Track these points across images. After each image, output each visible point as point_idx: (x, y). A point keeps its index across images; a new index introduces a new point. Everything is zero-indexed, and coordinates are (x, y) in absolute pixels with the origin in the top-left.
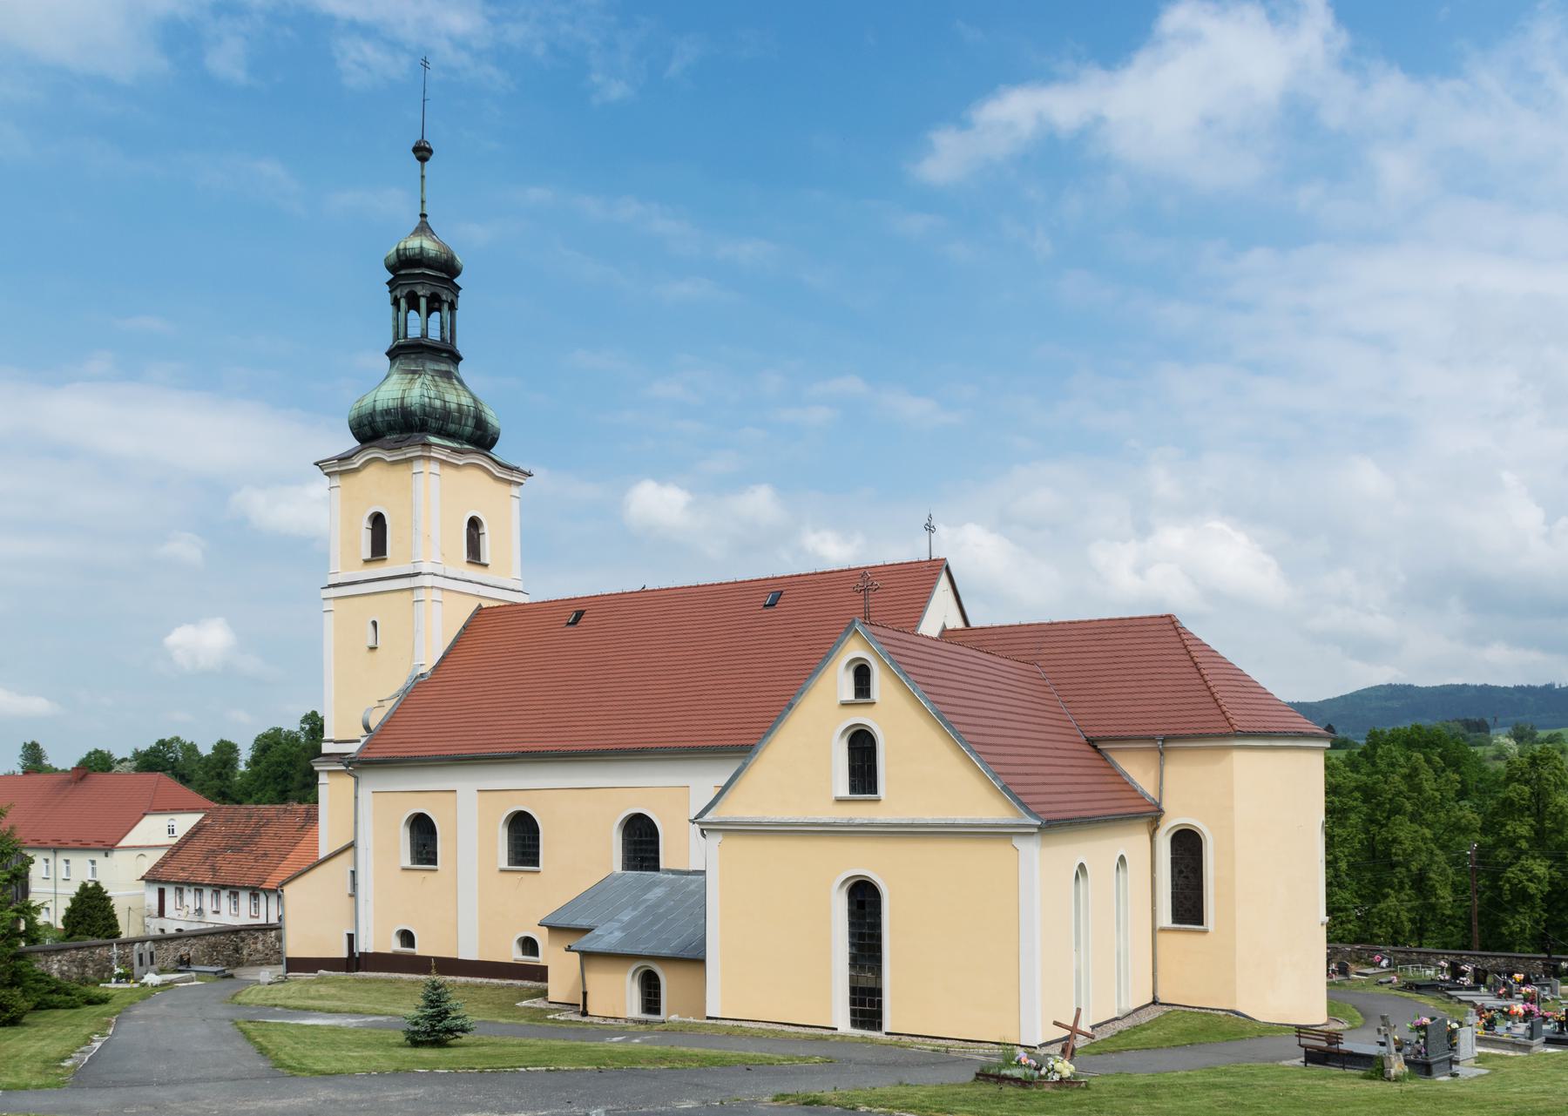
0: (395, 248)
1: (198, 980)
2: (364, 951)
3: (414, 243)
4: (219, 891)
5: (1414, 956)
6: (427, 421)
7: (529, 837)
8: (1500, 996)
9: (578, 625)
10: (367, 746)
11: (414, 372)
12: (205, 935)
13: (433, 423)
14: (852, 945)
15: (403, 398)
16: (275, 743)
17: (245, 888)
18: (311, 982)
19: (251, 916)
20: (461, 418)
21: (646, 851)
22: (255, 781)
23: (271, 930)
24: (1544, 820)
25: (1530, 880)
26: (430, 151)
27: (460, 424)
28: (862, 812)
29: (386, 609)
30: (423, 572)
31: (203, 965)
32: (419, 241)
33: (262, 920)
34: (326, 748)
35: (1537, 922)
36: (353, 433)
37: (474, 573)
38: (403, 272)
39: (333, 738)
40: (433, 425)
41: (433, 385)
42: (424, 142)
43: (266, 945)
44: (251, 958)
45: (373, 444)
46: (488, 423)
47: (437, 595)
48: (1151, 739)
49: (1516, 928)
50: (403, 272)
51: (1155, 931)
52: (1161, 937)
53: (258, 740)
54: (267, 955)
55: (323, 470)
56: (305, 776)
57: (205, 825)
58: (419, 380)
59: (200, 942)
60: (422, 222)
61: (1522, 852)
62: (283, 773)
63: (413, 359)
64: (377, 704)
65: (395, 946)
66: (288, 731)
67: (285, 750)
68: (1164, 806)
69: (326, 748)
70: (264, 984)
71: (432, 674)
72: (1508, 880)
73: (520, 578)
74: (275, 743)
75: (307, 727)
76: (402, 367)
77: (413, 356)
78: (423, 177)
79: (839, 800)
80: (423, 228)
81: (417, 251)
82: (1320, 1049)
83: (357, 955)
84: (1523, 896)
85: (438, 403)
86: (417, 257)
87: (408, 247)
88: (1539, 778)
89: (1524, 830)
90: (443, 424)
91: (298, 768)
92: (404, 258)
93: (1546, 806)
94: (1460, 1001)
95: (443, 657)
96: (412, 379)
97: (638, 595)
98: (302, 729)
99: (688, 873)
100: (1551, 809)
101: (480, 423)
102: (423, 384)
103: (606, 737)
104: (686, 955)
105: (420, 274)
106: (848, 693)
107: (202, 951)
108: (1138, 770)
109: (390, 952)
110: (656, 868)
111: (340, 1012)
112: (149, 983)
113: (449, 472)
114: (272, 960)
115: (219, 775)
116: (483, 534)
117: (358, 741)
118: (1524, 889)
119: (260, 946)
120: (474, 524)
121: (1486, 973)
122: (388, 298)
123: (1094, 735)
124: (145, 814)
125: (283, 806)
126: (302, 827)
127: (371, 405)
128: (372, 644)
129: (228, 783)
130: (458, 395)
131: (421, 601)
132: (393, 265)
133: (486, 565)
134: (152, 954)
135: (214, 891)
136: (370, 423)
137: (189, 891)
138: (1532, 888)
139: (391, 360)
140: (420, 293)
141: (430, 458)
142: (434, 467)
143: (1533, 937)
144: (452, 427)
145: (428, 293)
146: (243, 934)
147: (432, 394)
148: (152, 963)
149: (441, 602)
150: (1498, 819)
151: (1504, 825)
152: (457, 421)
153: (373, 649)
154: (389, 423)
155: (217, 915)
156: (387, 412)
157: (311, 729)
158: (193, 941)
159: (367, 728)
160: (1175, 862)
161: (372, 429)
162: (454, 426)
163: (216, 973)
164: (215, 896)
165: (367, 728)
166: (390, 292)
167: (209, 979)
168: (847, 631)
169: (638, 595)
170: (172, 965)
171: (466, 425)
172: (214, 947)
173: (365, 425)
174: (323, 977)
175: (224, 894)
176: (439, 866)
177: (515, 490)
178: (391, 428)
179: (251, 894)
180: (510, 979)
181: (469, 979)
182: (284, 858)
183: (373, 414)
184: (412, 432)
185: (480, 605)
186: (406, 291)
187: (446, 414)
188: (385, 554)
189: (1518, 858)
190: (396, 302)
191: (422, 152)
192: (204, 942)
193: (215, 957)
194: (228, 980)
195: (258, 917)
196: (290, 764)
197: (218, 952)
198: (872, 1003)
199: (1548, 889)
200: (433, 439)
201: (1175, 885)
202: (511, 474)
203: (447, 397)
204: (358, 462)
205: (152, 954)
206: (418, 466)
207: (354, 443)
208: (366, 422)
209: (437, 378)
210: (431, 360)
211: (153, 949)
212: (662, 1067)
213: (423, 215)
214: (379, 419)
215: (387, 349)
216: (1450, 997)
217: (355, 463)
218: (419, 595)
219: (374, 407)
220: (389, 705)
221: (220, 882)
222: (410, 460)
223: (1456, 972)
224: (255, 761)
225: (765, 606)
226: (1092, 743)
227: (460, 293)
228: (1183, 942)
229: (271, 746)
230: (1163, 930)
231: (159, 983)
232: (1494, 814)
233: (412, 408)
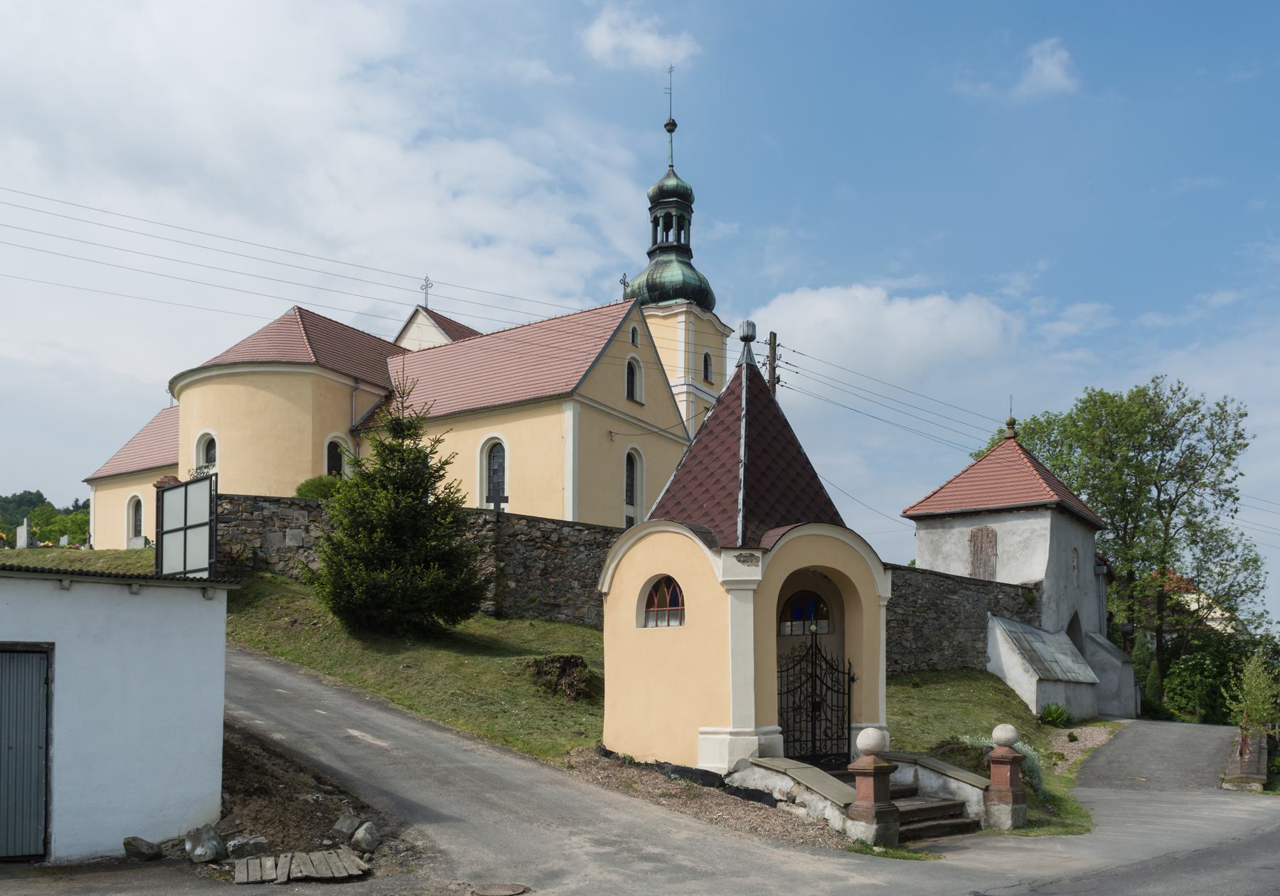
80: (672, 173)
190: (655, 222)
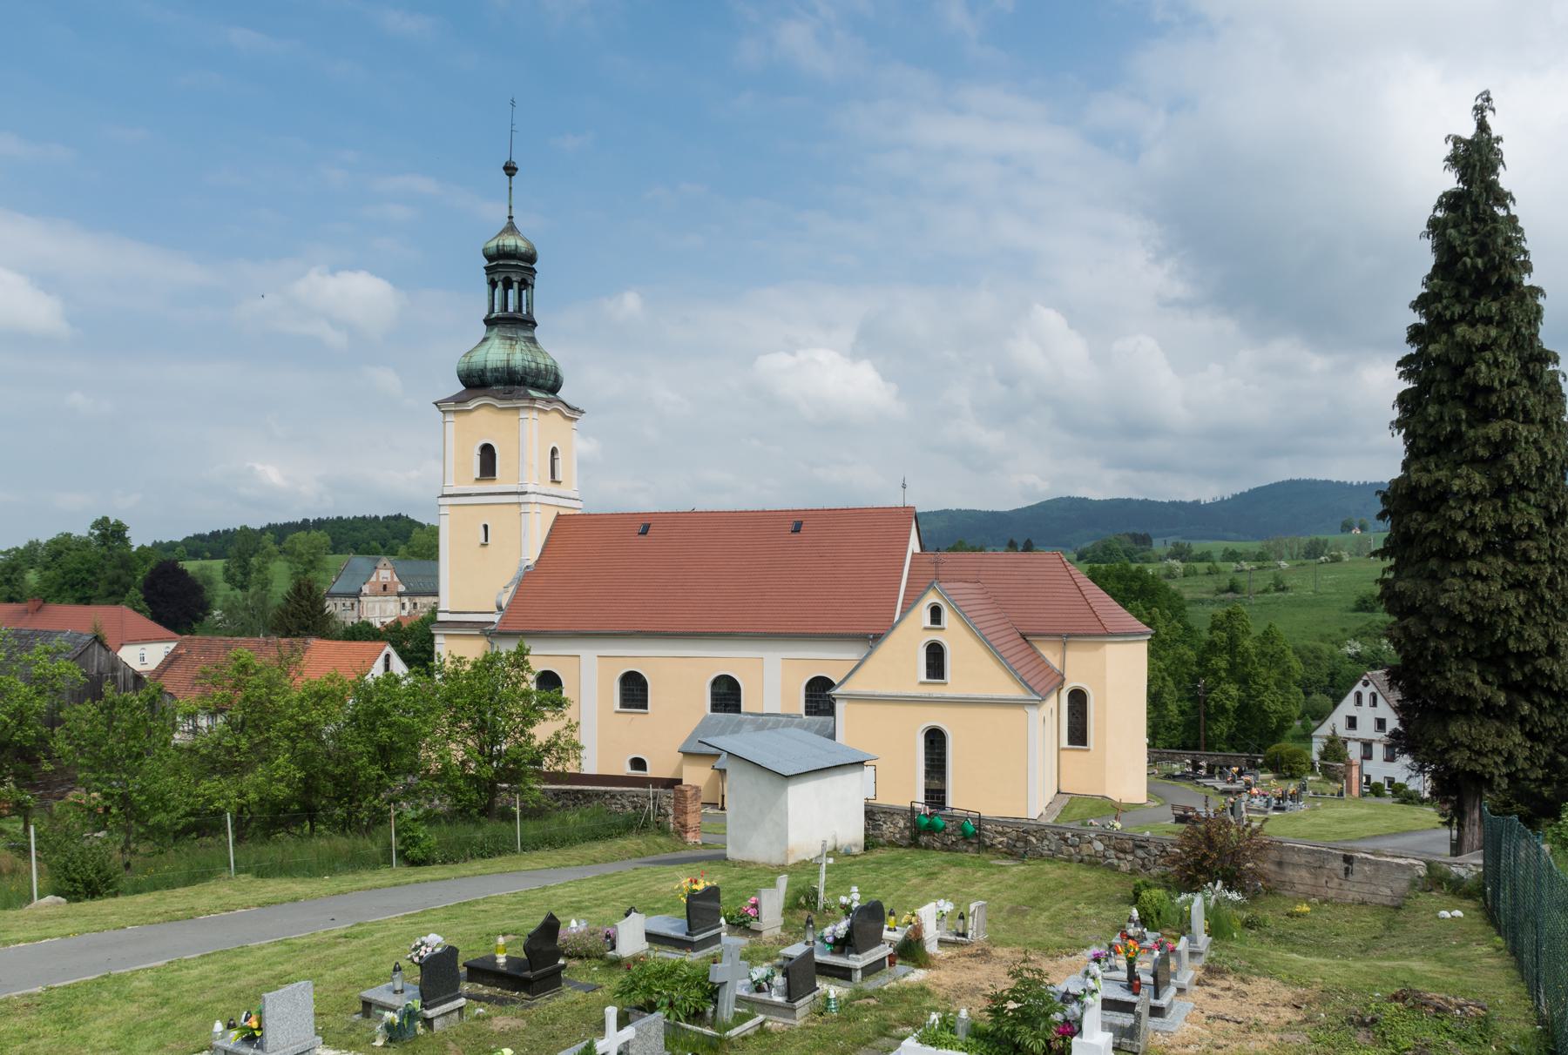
5: (1165, 755)
8: (1228, 782)
11: (511, 339)
13: (529, 380)
14: (927, 765)
16: (67, 549)
21: (729, 700)
22: (50, 587)
24: (1235, 656)
25: (1227, 699)
28: (936, 690)
29: (500, 519)
30: (529, 491)
34: (441, 617)
35: (1230, 728)
37: (554, 489)
39: (448, 609)
47: (538, 508)
48: (1059, 635)
49: (1218, 732)
51: (1059, 749)
52: (1062, 753)
57: (181, 654)
60: (509, 223)
61: (1221, 679)
65: (627, 770)
68: (1065, 676)
69: (441, 617)
72: (1213, 699)
74: (67, 549)
76: (500, 333)
78: (510, 188)
79: (922, 683)
80: (511, 228)
81: (513, 248)
82: (1181, 815)
84: (1222, 710)
85: (533, 365)
88: (1232, 627)
89: (1223, 664)
93: (1237, 646)
94: (1205, 786)
99: (762, 715)
100: (1240, 649)
106: (927, 622)
108: (1050, 654)
110: (737, 709)
113: (542, 416)
115: (8, 581)
118: (1224, 705)
120: (554, 451)
121: (1214, 766)
123: (1024, 631)
124: (122, 645)
129: (18, 589)
133: (559, 482)
138: (1228, 704)
140: (514, 279)
141: (533, 408)
142: (535, 414)
143: (1228, 737)
145: (519, 279)
150: (1206, 655)
151: (1211, 660)
153: (483, 545)
154: (496, 378)
156: (496, 370)
157: (102, 535)
160: (1070, 708)
168: (929, 588)
177: (574, 425)
178: (497, 381)
186: (503, 276)
189: (1219, 683)
190: (493, 284)
191: (510, 170)
196: (88, 571)
198: (938, 798)
199: (1237, 705)
200: (534, 393)
201: (1070, 722)
202: (572, 412)
203: (539, 360)
206: (523, 414)
210: (521, 329)
213: (510, 217)
214: (489, 374)
216: (1198, 783)
218: (524, 508)
220: (511, 589)
222: (518, 408)
223: (1196, 767)
226: (1023, 636)
228: (1075, 756)
230: (1064, 749)
232: (1204, 652)
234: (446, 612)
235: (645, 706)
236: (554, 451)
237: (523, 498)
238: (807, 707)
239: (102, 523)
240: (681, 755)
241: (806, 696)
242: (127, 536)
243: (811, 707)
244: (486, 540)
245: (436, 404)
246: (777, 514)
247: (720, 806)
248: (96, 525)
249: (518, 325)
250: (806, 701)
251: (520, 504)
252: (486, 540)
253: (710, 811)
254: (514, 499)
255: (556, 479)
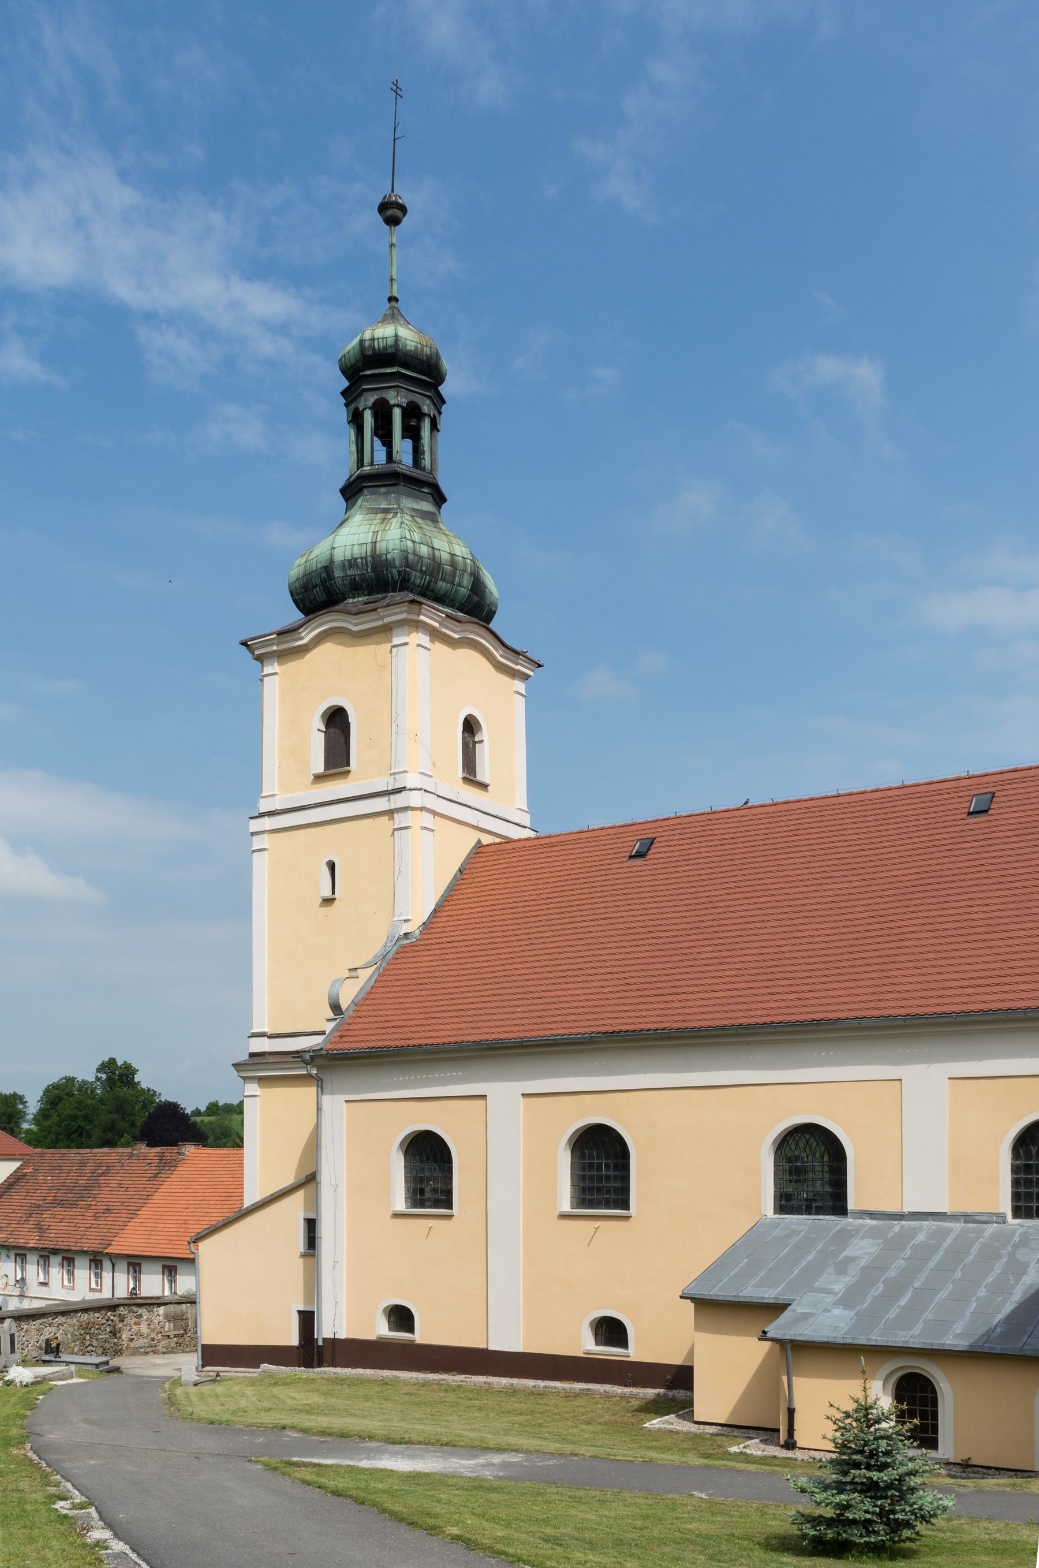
0: (356, 340)
1: (80, 1376)
2: (331, 1336)
3: (385, 332)
4: (48, 1257)
6: (409, 574)
7: (607, 1166)
9: (647, 857)
10: (341, 1034)
11: (386, 511)
12: (76, 1311)
15: (374, 543)
17: (83, 1253)
18: (252, 1382)
19: (91, 1290)
20: (454, 575)
23: (159, 1305)
26: (403, 209)
27: (452, 583)
30: (408, 786)
31: (73, 1353)
32: (393, 328)
33: (106, 1294)
36: (295, 601)
37: (470, 795)
38: (368, 372)
40: (418, 581)
41: (416, 526)
42: (396, 196)
43: (152, 1326)
44: (132, 1345)
45: (333, 609)
46: (486, 587)
47: (427, 820)
50: (368, 372)
53: (47, 1091)
54: (153, 1339)
55: (252, 653)
56: (104, 1131)
57: (25, 1174)
58: (395, 520)
59: (69, 1321)
60: (391, 308)
62: (78, 1128)
63: (384, 493)
64: (348, 974)
65: (381, 1329)
66: (83, 1080)
67: (80, 1102)
70: (187, 1384)
71: (421, 933)
73: (526, 809)
75: (104, 1076)
77: (383, 490)
81: (390, 342)
83: (320, 1343)
85: (424, 550)
86: (389, 351)
87: (376, 336)
90: (430, 581)
91: (96, 1123)
92: (370, 352)
95: (435, 911)
96: (384, 519)
97: (736, 813)
98: (98, 1079)
99: (901, 1217)
101: (478, 586)
102: (402, 523)
103: (750, 999)
104: (987, 1347)
105: (395, 373)
107: (73, 1335)
109: (373, 1338)
110: (837, 1204)
111: (410, 1442)
112: (17, 1380)
113: (439, 647)
114: (160, 1348)
116: (482, 741)
117: (323, 1033)
119: (144, 1328)
120: (470, 726)
122: (342, 414)
125: (129, 1150)
126: (156, 1176)
127: (326, 556)
128: (328, 893)
130: (450, 543)
131: (407, 828)
132: (352, 366)
133: (484, 786)
134: (12, 1336)
135: (41, 1256)
136: (324, 582)
137: (8, 1256)
139: (346, 500)
140: (392, 402)
142: (420, 638)
144: (442, 586)
145: (404, 402)
146: (122, 1310)
147: (417, 537)
148: (13, 1351)
149: (432, 830)
152: (448, 577)
153: (328, 901)
154: (353, 579)
155: (44, 1288)
156: (352, 563)
157: (109, 1079)
158: (61, 1319)
159: (336, 1008)
161: (328, 590)
162: (444, 584)
163: (97, 1365)
164: (42, 1262)
165: (336, 1008)
166: (347, 405)
167: (91, 1375)
169: (736, 813)
170: (34, 1354)
171: (460, 585)
172: (87, 1328)
173: (315, 586)
174: (271, 1375)
175: (55, 1260)
176: (455, 1210)
178: (356, 587)
179: (91, 1261)
180: (230, 1367)
181: (515, 1381)
182: (134, 1214)
183: (328, 569)
184: (387, 591)
185: (479, 842)
187: (434, 567)
188: (348, 765)
190: (356, 419)
192: (75, 1320)
193: (88, 1343)
194: (115, 1375)
195: (100, 1291)
196: (86, 1118)
197: (92, 1335)
203: (437, 544)
204: (307, 636)
205: (12, 1336)
207: (297, 616)
208: (318, 582)
209: (418, 520)
210: (408, 495)
211: (14, 1330)
212: (675, 1496)
214: (338, 574)
215: (342, 483)
217: (302, 638)
218: (400, 819)
219: (332, 556)
220: (365, 975)
221: (48, 1244)
224: (43, 1115)
225: (970, 814)
227: (444, 408)
229: (63, 1099)
231: (30, 1380)
233: (389, 556)
234: (262, 1035)
235: (624, 1203)
236: (470, 726)
237: (397, 801)
238: (1016, 1196)
239: (109, 1066)
240: (689, 1305)
241: (1015, 1169)
242: (136, 1080)
243: (1029, 1196)
244: (333, 893)
245: (244, 644)
246: (934, 787)
247: (783, 1436)
248: (103, 1067)
249: (400, 488)
250: (1016, 1183)
251: (390, 813)
252: (333, 893)
253: (755, 1447)
254: (381, 804)
255: (479, 777)
